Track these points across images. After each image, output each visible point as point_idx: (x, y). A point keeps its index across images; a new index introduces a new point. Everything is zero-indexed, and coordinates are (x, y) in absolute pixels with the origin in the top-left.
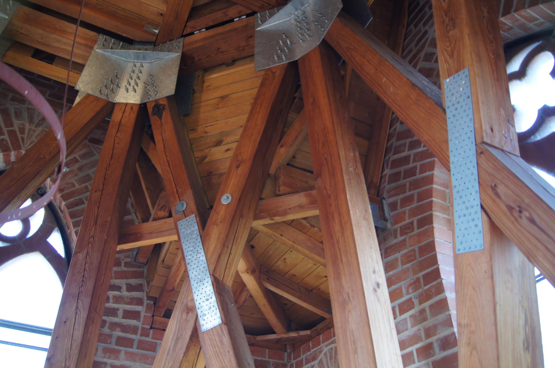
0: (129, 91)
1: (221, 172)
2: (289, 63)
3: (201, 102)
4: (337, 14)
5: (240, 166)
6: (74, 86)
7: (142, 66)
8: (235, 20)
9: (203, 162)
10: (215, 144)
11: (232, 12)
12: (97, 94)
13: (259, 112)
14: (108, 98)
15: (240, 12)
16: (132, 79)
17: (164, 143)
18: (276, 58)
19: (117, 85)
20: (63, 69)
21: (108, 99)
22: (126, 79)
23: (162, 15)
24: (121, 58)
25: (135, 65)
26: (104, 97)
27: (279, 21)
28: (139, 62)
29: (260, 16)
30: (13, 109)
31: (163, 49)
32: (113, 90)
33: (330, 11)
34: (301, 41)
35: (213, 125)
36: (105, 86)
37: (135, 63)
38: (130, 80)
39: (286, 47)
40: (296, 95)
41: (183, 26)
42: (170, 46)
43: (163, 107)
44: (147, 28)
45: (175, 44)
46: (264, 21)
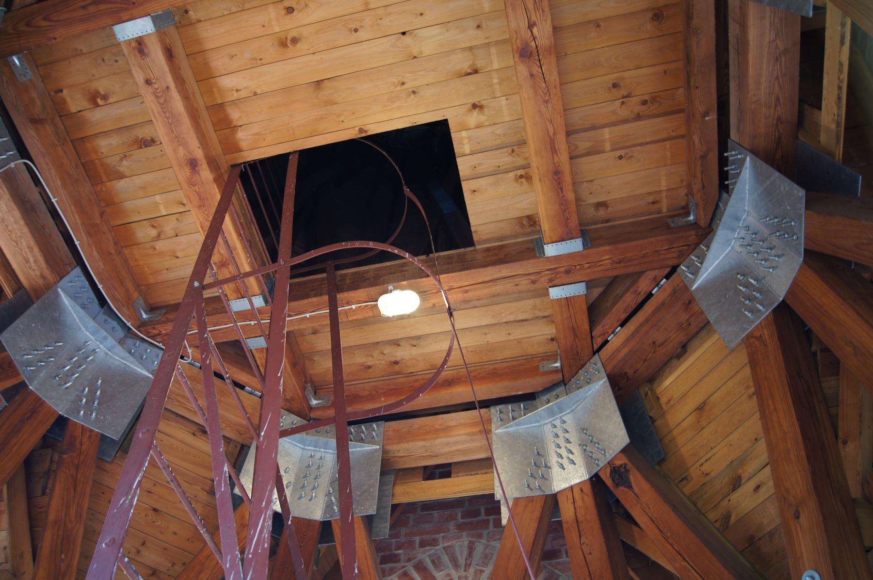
0: (565, 467)
1: (768, 530)
2: (774, 310)
3: (671, 431)
4: (803, 206)
5: (799, 513)
6: (493, 492)
7: (565, 422)
8: (654, 292)
9: (730, 525)
10: (731, 487)
11: (643, 285)
12: (528, 493)
13: (775, 409)
15: (655, 279)
16: (560, 448)
17: (656, 525)
18: (750, 315)
19: (545, 467)
20: (466, 477)
21: (544, 492)
22: (552, 451)
23: (552, 339)
24: (532, 425)
25: (554, 425)
26: (537, 493)
27: (718, 259)
28: (557, 418)
29: (686, 267)
30: (428, 559)
31: (579, 383)
32: (543, 476)
33: (789, 208)
34: (771, 270)
35: (711, 457)
36: (531, 476)
37: (553, 423)
38: (559, 450)
39: (754, 291)
40: (814, 348)
41: (589, 340)
42: (586, 374)
43: (625, 468)
44: (543, 366)
45: (591, 370)
46: (696, 272)
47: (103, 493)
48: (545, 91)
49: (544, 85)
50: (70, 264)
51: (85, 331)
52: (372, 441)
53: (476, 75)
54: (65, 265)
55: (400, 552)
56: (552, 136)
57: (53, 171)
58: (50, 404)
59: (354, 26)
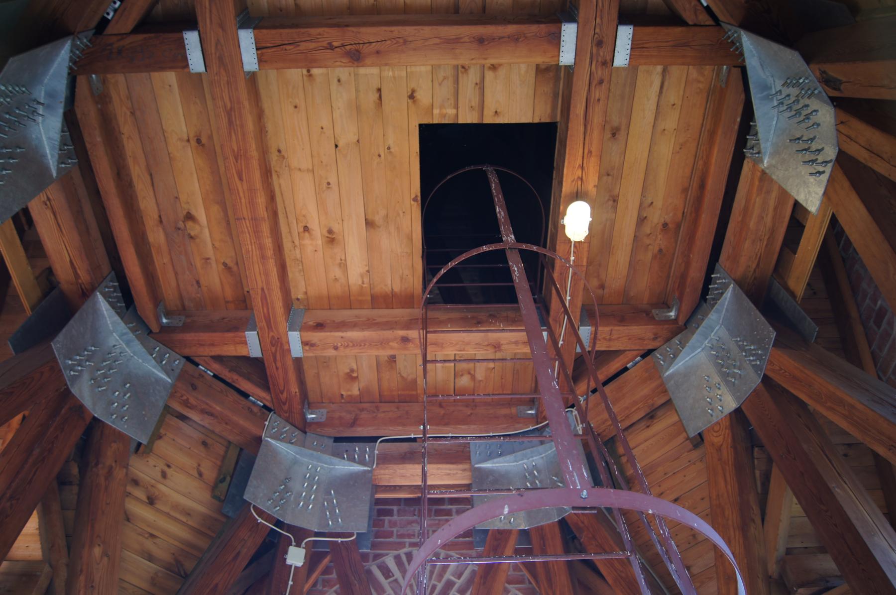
12: (825, 178)
14: (830, 161)
19: (812, 142)
26: (828, 169)
47: (639, 527)
48: (395, 42)
49: (389, 42)
50: (465, 447)
51: (518, 463)
52: (725, 287)
53: (382, 90)
54: (463, 451)
55: (879, 303)
56: (442, 41)
57: (391, 428)
58: (546, 523)
59: (325, 185)
